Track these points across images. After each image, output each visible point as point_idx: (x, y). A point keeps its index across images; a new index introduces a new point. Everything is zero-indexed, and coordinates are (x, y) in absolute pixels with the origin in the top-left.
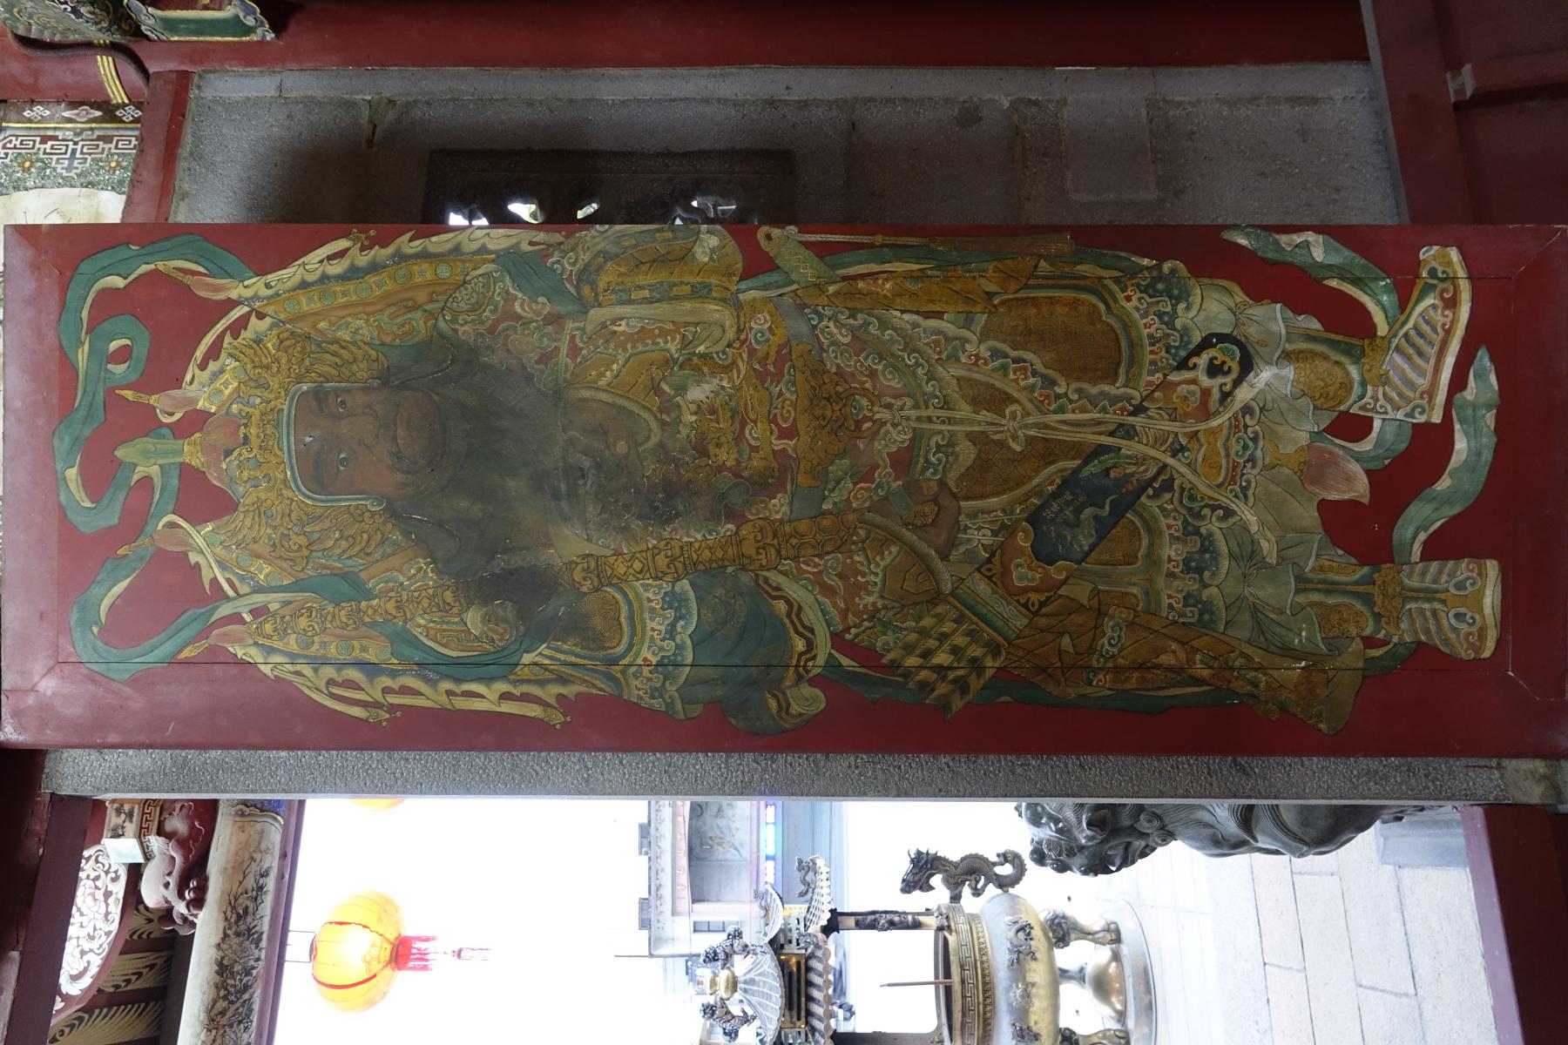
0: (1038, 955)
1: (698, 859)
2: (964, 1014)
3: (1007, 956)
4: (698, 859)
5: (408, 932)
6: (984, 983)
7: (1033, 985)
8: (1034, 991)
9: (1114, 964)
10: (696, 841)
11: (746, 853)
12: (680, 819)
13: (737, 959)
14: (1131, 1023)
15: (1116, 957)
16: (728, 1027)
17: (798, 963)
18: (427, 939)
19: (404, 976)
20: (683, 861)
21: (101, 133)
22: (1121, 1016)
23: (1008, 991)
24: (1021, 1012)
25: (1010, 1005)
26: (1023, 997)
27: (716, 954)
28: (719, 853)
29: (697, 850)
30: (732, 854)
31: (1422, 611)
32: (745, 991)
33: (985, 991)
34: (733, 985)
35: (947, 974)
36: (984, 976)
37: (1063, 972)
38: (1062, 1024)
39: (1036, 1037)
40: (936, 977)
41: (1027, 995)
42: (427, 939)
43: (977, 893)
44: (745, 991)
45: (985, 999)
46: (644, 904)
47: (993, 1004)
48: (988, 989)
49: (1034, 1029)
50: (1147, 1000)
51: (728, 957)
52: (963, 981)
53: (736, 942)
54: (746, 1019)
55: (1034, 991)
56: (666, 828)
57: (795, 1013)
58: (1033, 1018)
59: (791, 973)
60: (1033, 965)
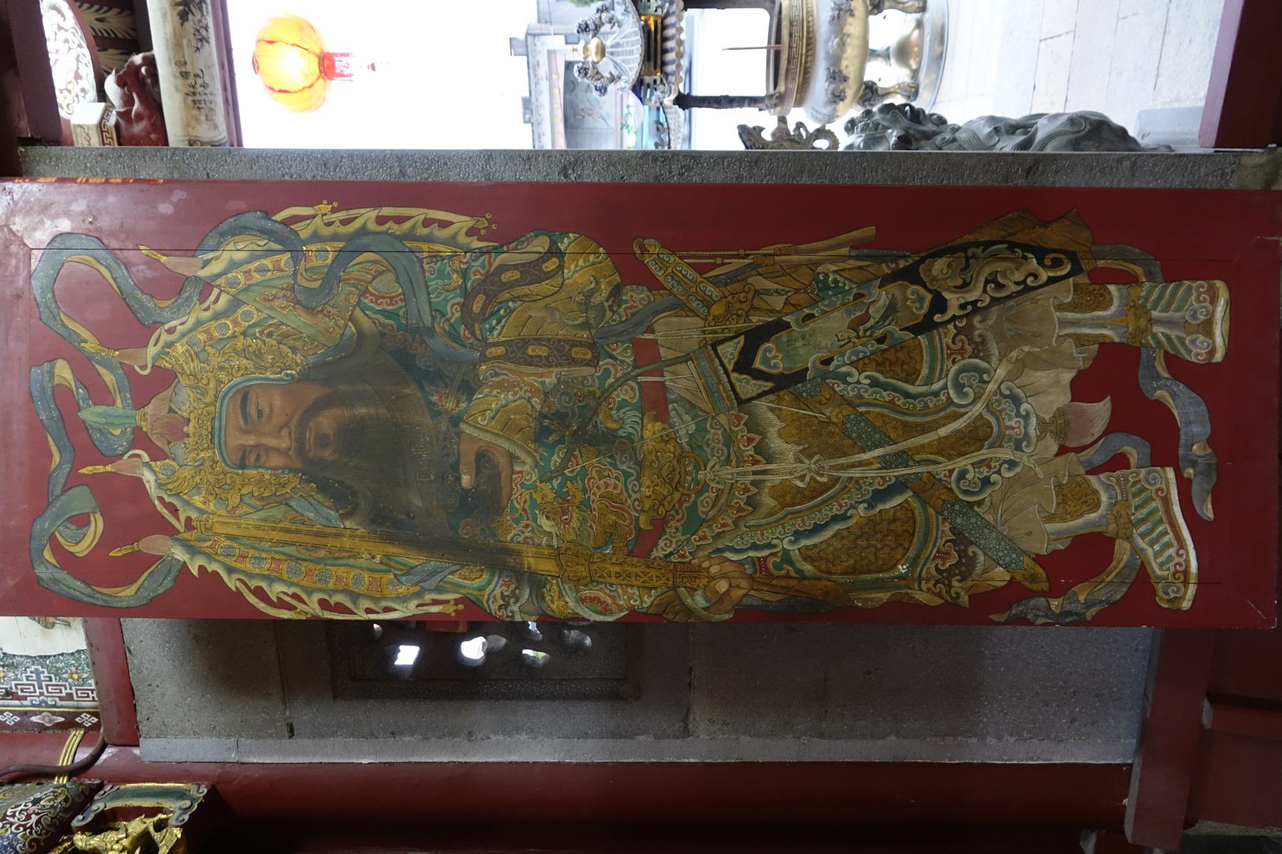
0: (856, 13)
1: (572, 127)
2: (789, 62)
3: (830, 13)
4: (572, 127)
5: (330, 49)
6: (808, 38)
7: (849, 35)
8: (848, 40)
9: (917, 32)
10: (570, 113)
11: (612, 122)
12: (556, 91)
13: (606, 28)
14: (922, 76)
15: (919, 25)
16: (599, 84)
17: (656, 23)
18: (346, 55)
19: (335, 84)
20: (560, 127)
21: (24, 702)
22: (915, 74)
23: (827, 42)
24: (835, 60)
25: (828, 53)
26: (838, 45)
27: (587, 26)
28: (589, 122)
29: (571, 120)
30: (600, 124)
31: (1157, 555)
32: (612, 54)
33: (808, 45)
34: (602, 51)
35: (778, 41)
36: (808, 32)
37: (873, 51)
38: (866, 78)
39: (845, 79)
40: (769, 42)
41: (842, 45)
42: (346, 55)
43: (800, 125)
44: (612, 54)
45: (807, 51)
46: (527, 104)
47: (813, 55)
48: (811, 43)
49: (845, 72)
50: (939, 50)
51: (597, 27)
52: (791, 35)
53: (604, 15)
54: (613, 79)
55: (848, 40)
56: (545, 99)
57: (652, 64)
58: (844, 63)
59: (649, 31)
60: (850, 20)
